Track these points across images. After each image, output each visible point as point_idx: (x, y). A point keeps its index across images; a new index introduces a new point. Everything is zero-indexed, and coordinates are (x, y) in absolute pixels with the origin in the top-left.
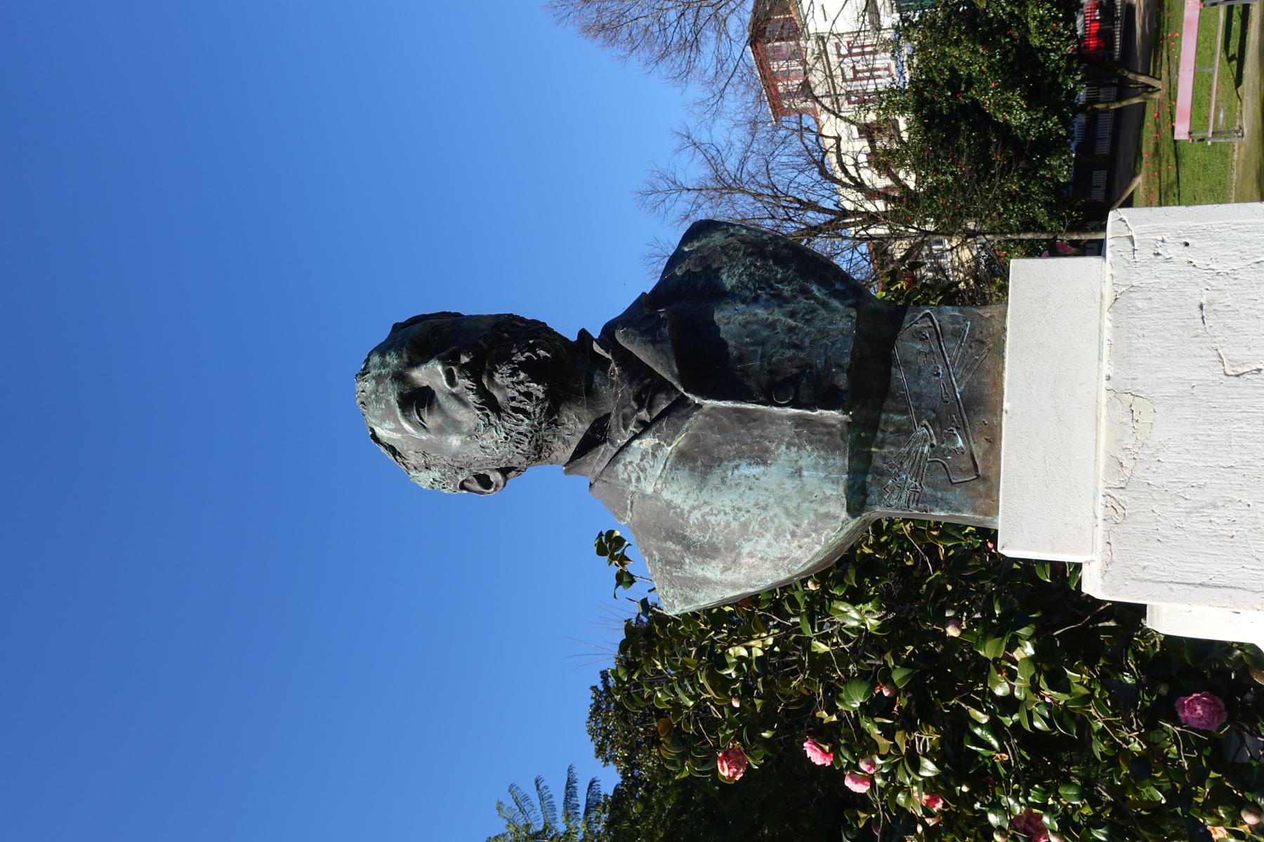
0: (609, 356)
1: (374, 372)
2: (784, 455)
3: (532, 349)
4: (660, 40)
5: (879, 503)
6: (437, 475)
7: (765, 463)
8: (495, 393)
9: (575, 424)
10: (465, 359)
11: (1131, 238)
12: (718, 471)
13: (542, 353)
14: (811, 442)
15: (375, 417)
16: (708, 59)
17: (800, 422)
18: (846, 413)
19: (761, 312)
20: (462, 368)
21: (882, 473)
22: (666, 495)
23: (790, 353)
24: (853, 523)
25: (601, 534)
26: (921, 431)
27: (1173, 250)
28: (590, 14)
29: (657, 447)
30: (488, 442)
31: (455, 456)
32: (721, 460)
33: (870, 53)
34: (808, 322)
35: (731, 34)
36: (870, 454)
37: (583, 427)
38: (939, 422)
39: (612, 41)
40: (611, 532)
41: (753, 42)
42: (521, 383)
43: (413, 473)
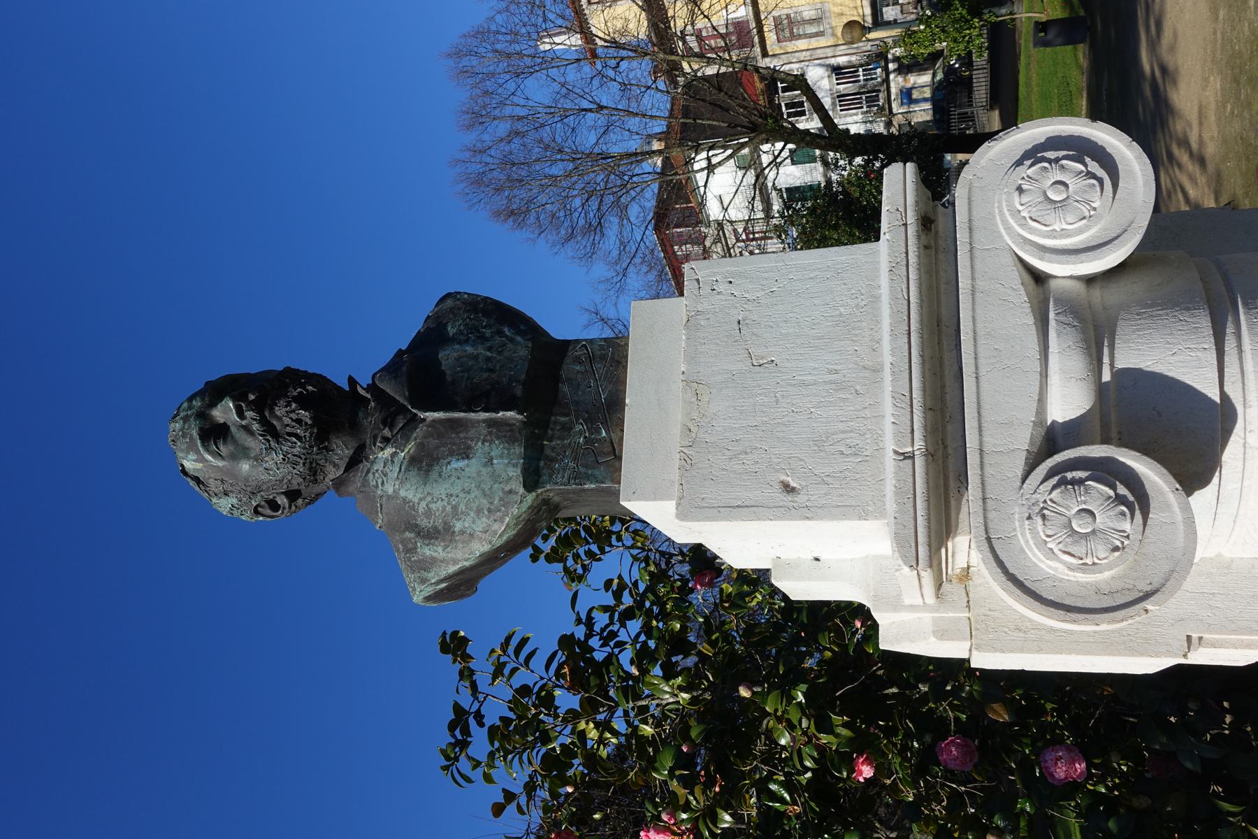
0: (369, 396)
1: (182, 414)
2: (480, 448)
3: (303, 386)
4: (566, 224)
5: (549, 482)
6: (235, 501)
7: (468, 457)
8: (275, 423)
9: (342, 450)
10: (252, 397)
11: (698, 280)
12: (437, 468)
13: (310, 388)
14: (498, 438)
15: (182, 451)
16: (612, 242)
17: (491, 423)
18: (520, 413)
19: (469, 349)
20: (249, 403)
21: (552, 460)
22: (402, 493)
23: (485, 375)
24: (530, 498)
25: (445, 633)
26: (578, 428)
27: (721, 287)
28: (500, 201)
29: (394, 455)
30: (270, 464)
31: (246, 479)
32: (438, 459)
33: (761, 239)
34: (500, 353)
35: (632, 219)
36: (543, 446)
37: (348, 452)
38: (590, 421)
39: (521, 225)
40: (455, 633)
41: (656, 228)
42: (293, 411)
43: (214, 500)
